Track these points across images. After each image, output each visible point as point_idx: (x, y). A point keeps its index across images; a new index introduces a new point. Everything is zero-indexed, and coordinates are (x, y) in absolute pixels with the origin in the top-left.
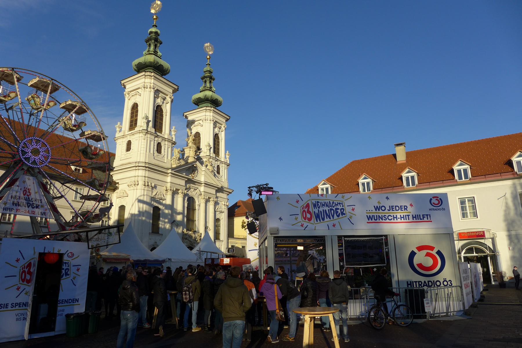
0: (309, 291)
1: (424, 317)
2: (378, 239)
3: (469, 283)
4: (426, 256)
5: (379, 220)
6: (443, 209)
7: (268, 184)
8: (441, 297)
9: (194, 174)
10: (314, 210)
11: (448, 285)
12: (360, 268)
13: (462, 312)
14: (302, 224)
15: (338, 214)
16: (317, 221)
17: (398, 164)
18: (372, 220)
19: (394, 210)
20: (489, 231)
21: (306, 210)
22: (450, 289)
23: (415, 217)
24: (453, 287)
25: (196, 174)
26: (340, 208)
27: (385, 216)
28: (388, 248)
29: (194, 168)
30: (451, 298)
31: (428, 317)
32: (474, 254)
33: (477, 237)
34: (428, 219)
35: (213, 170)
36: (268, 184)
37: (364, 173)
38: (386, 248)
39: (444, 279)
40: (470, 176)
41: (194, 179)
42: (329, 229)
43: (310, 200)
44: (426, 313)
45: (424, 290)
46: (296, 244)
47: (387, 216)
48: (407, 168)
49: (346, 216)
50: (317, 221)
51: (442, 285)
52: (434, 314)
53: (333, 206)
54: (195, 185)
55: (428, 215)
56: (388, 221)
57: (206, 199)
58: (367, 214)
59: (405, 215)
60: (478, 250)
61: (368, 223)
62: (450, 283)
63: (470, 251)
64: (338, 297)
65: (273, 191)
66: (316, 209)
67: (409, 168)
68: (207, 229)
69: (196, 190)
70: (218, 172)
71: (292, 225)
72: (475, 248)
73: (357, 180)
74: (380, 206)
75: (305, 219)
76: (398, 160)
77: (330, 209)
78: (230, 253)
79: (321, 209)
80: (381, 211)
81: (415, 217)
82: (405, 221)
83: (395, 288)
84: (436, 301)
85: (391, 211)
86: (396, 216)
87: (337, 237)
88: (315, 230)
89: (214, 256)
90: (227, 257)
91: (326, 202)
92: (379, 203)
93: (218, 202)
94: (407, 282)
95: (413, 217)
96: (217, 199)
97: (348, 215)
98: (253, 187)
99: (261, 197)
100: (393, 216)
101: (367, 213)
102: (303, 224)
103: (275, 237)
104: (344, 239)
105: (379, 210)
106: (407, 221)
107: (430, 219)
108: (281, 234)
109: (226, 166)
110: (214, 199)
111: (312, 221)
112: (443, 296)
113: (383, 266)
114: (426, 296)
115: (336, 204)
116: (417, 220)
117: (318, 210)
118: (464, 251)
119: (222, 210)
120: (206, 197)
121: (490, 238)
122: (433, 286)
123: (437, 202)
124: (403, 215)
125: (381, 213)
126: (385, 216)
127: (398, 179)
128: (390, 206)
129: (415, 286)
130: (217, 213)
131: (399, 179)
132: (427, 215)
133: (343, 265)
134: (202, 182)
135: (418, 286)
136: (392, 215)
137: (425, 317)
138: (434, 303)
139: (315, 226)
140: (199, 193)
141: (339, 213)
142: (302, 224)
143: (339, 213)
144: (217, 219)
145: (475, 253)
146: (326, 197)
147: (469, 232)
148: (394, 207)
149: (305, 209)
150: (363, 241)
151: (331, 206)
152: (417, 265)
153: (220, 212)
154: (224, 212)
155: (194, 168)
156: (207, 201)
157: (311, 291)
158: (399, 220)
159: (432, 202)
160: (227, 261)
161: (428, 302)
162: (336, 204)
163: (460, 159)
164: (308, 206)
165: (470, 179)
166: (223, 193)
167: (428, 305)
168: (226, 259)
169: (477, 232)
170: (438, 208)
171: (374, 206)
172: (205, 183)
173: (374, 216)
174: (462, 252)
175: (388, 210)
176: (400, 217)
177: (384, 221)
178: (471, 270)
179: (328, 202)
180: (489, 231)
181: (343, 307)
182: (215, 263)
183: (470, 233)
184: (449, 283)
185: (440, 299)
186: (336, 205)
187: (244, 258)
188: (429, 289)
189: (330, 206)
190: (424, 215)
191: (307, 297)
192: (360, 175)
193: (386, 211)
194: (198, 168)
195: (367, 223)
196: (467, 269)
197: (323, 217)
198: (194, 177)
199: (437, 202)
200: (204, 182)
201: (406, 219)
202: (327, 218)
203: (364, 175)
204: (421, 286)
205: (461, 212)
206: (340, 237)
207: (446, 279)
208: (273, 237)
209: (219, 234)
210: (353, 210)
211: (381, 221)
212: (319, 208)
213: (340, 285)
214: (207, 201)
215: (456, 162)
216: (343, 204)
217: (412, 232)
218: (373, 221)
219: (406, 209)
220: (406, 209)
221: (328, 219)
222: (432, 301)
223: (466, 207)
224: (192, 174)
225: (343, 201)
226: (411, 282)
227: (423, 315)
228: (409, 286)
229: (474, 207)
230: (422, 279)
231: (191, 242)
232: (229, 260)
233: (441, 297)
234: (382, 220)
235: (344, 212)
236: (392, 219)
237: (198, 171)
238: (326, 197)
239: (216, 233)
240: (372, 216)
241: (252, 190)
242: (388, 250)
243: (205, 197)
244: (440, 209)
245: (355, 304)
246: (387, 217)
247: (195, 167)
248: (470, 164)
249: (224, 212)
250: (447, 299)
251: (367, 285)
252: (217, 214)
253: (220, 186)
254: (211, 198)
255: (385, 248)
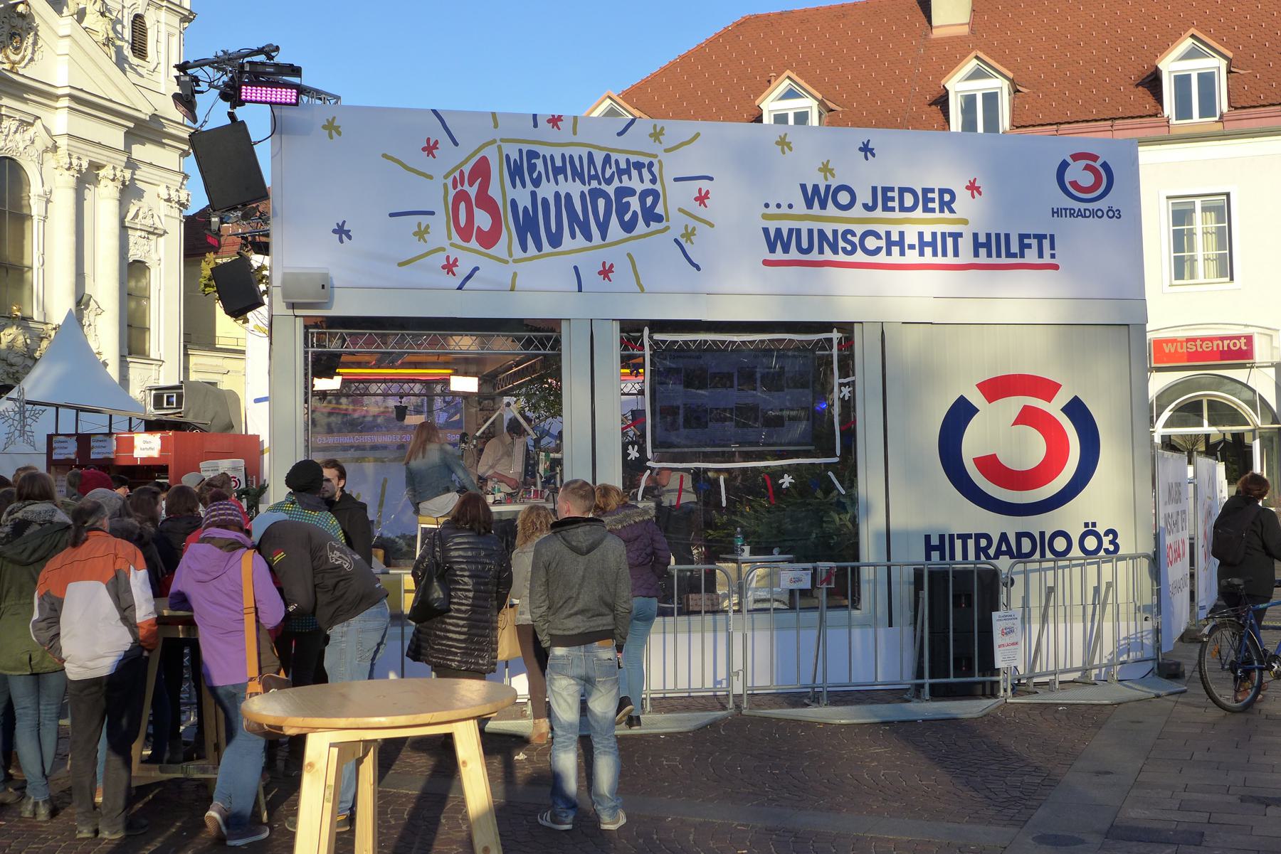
0: (458, 583)
1: (988, 691)
2: (809, 342)
3: (1183, 542)
4: (1015, 423)
5: (821, 251)
6: (1111, 214)
7: (277, 49)
8: (1068, 603)
9: (17, 49)
10: (512, 193)
11: (1102, 553)
12: (718, 471)
13: (1150, 665)
14: (448, 258)
15: (627, 218)
16: (525, 249)
17: (934, 40)
18: (786, 249)
19: (893, 209)
20: (1269, 332)
21: (473, 191)
22: (1107, 568)
23: (987, 245)
24: (1123, 558)
25: (30, 50)
26: (639, 188)
27: (849, 237)
28: (854, 381)
29: (19, 22)
30: (1109, 609)
31: (1005, 690)
32: (1201, 425)
33: (954, 596)
34: (1041, 255)
35: (111, 35)
36: (277, 49)
37: (788, 73)
38: (844, 385)
39: (1086, 525)
40: (1223, 104)
41: (17, 73)
42: (580, 290)
43: (494, 141)
44: (999, 675)
45: (995, 573)
46: (445, 365)
47: (858, 236)
48: (973, 54)
49: (667, 228)
50: (525, 249)
51: (1076, 551)
52: (1030, 678)
53: (607, 176)
54: (25, 101)
55: (1044, 236)
56: (860, 256)
57: (79, 171)
58: (767, 224)
59: (943, 235)
60: (1222, 413)
61: (767, 263)
62: (1112, 542)
63: (1190, 412)
64: (576, 614)
65: (301, 90)
66: (524, 185)
67: (981, 55)
68: (87, 305)
69: (32, 125)
70: (139, 49)
71: (401, 264)
72: (1211, 403)
73: (757, 103)
74: (828, 187)
75: (465, 234)
76: (935, 22)
77: (590, 191)
78: (167, 413)
79: (547, 190)
80: (831, 210)
81: (987, 245)
82: (940, 260)
83: (868, 565)
84: (1044, 619)
85: (879, 213)
86: (902, 234)
87: (616, 326)
88: (512, 290)
89: (90, 424)
90: (151, 426)
91: (571, 157)
92: (826, 169)
93: (139, 184)
94: (928, 538)
95: (977, 246)
96: (133, 174)
97: (676, 223)
98: (200, 64)
99: (240, 113)
100: (888, 234)
101: (765, 217)
102: (456, 260)
103: (311, 325)
104: (651, 338)
105: (823, 206)
106: (950, 259)
107: (1053, 256)
108: (343, 307)
109: (177, 19)
110: (119, 174)
111: (500, 249)
112: (1077, 599)
113: (826, 464)
114: (1003, 598)
115: (623, 165)
116: (994, 260)
117: (534, 194)
118: (1166, 414)
119: (158, 225)
120: (79, 158)
121: (1272, 366)
122: (1037, 555)
123: (1087, 179)
124: (934, 235)
125: (831, 220)
126: (849, 237)
127: (930, 105)
128: (874, 189)
129: (959, 556)
130: (134, 237)
131: (934, 103)
132: (1040, 238)
133: (642, 459)
134: (59, 92)
135: (971, 556)
136: (881, 229)
137: (991, 691)
138: (1035, 628)
139: (515, 274)
140: (43, 141)
141: (635, 213)
142: (448, 258)
143: (635, 213)
144: (135, 261)
145: (1206, 422)
146: (575, 133)
147: (1194, 340)
148: (896, 194)
149: (466, 187)
150: (739, 348)
151: (596, 177)
152: (975, 460)
153: (149, 233)
154: (165, 232)
155: (19, 22)
156: (86, 179)
157: (466, 579)
158: (912, 257)
159: (1068, 177)
160: (147, 446)
161: (1009, 624)
162: (623, 165)
163: (1193, 31)
164: (481, 171)
165: (1222, 116)
166: (163, 145)
167: (1007, 639)
168: (146, 436)
169: (1222, 339)
170: (1090, 206)
171: (803, 187)
172: (72, 97)
173: (799, 231)
174: (1158, 417)
175: (866, 206)
176: (916, 242)
177: (842, 257)
178: (1196, 487)
179: (580, 158)
180: (1271, 336)
181: (599, 660)
182: (92, 457)
183: (1199, 343)
184: (1106, 544)
185: (1061, 611)
186: (621, 172)
187: (232, 432)
188: (1020, 567)
189: (591, 178)
190: (1028, 236)
191: (444, 612)
192: (769, 81)
193: (858, 211)
194: (37, 20)
195: (766, 263)
196: (1182, 485)
197: (554, 230)
198: (19, 62)
199: (1087, 179)
200: (68, 91)
201: (945, 254)
202: (573, 236)
203: (788, 82)
204: (988, 557)
205: (1173, 255)
206: (631, 330)
207: (1094, 525)
208: (300, 323)
209: (144, 330)
210: (702, 198)
211: (828, 255)
212: (536, 183)
213: (589, 551)
214: (86, 179)
215: (1173, 42)
216: (655, 169)
217: (970, 312)
218: (794, 254)
219: (946, 205)
220: (946, 205)
221: (580, 240)
222: (1026, 619)
223: (1191, 233)
224: (9, 52)
225: (656, 156)
226: (942, 537)
227: (983, 683)
228: (935, 555)
229: (1225, 238)
230: (994, 524)
231: (11, 365)
232: (159, 442)
233: (1068, 603)
234: (835, 252)
235: (659, 209)
236: (878, 250)
237: (36, 34)
238: (575, 133)
239: (129, 326)
240: (791, 231)
241: (196, 80)
242: (853, 393)
243: (75, 162)
244: (1100, 213)
245: (670, 637)
246: (856, 240)
247: (21, 15)
248: (1230, 55)
249: (165, 232)
250: (1090, 609)
251: (747, 549)
252: (132, 240)
253: (145, 112)
254: (103, 166)
255: (841, 385)
